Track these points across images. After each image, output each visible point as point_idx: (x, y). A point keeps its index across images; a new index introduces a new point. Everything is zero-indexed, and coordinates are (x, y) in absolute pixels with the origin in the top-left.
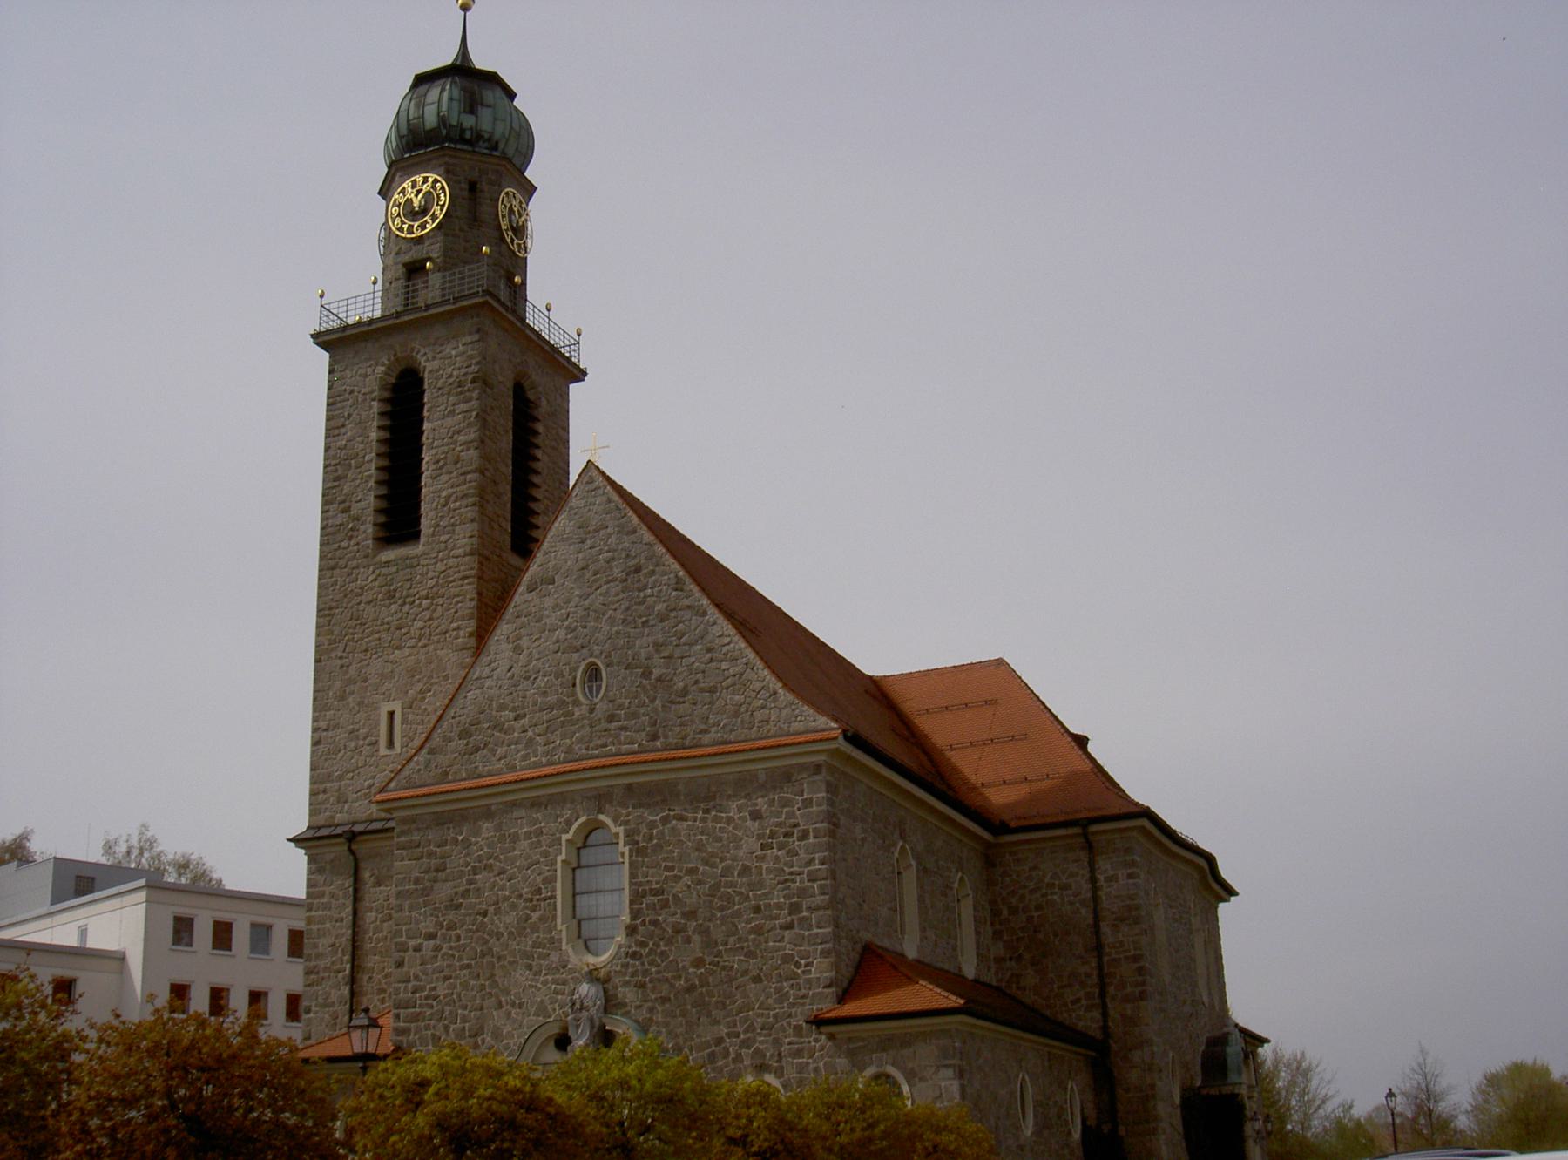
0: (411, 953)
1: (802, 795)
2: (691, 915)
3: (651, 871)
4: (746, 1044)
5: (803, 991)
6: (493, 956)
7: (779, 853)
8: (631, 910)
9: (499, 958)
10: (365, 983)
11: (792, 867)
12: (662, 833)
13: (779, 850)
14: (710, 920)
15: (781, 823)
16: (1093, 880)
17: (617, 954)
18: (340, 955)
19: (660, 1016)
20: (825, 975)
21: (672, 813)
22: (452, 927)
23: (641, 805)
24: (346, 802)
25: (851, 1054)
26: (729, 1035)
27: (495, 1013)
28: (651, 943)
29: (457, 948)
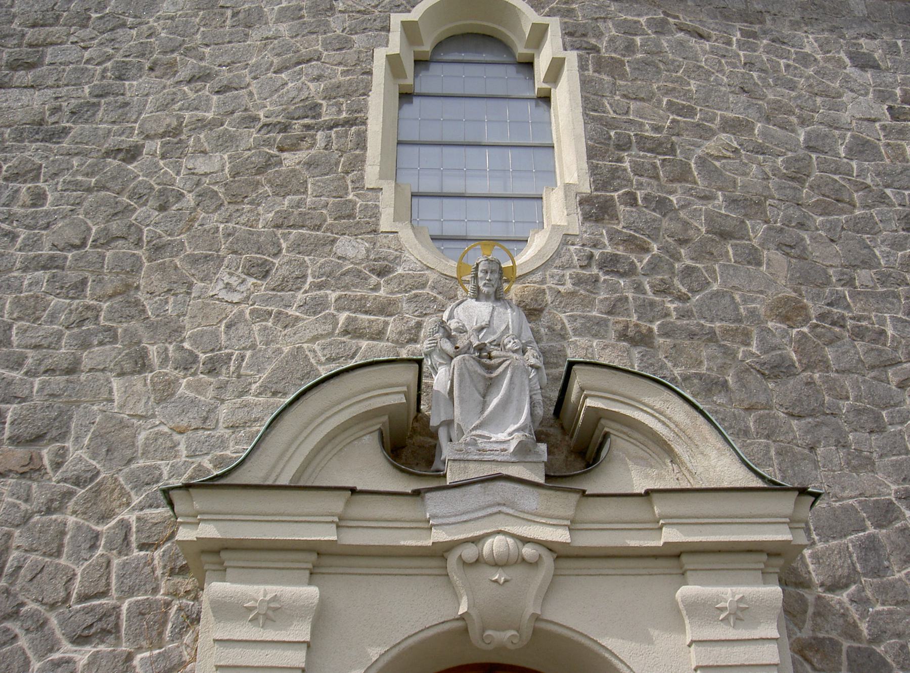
3: (633, 105)
9: (157, 249)
17: (557, 254)
27: (116, 383)
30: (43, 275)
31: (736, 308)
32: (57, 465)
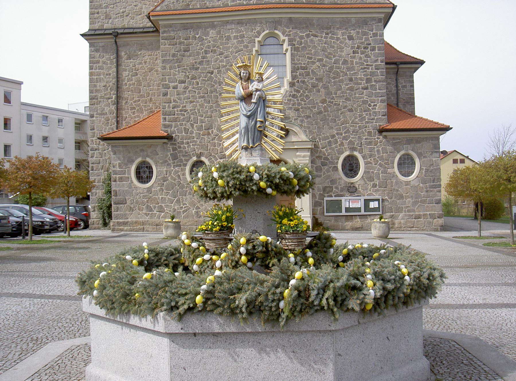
0: (171, 89)
1: (373, 31)
2: (320, 80)
3: (301, 58)
4: (345, 138)
5: (372, 117)
6: (217, 93)
7: (362, 56)
8: (292, 75)
10: (124, 104)
11: (367, 62)
12: (307, 41)
13: (361, 54)
14: (329, 83)
15: (362, 42)
16: (397, 86)
18: (109, 91)
19: (306, 124)
20: (383, 110)
21: (311, 33)
22: (194, 78)
23: (296, 28)
24: (110, 18)
25: (394, 145)
26: (337, 134)
27: (218, 119)
28: (301, 91)
29: (198, 88)
30: (202, 99)
31: (314, 101)
32: (212, 133)
